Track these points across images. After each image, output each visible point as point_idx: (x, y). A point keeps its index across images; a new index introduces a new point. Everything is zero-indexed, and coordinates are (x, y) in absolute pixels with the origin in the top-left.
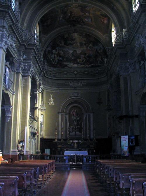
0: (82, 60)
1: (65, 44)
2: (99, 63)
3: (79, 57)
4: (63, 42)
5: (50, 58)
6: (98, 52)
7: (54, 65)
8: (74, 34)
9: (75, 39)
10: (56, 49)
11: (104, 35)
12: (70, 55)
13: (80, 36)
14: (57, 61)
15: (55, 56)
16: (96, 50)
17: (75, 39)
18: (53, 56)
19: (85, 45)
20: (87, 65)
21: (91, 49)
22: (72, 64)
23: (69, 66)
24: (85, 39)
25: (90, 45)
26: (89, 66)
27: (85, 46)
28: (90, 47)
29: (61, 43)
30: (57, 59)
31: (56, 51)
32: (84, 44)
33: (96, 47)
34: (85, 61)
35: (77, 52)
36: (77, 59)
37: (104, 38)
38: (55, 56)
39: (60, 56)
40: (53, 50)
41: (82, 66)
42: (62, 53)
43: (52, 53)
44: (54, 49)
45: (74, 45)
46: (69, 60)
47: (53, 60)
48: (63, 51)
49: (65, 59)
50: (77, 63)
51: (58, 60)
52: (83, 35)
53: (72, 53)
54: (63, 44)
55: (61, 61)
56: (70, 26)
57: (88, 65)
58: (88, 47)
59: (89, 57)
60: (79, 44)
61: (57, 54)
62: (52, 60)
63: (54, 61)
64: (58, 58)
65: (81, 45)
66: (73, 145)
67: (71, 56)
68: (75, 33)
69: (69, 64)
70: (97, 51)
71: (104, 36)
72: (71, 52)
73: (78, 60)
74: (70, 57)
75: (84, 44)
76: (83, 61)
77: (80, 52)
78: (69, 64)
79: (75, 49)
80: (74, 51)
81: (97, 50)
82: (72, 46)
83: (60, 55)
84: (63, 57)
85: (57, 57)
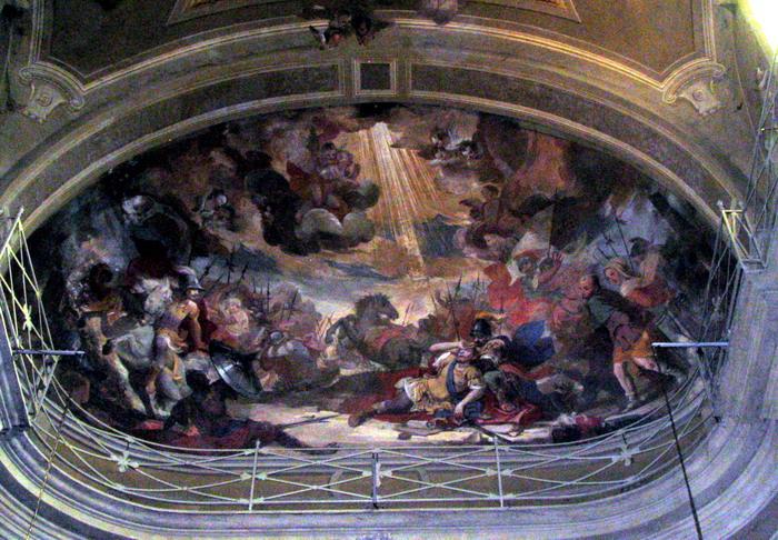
0: (450, 384)
1: (271, 235)
2: (629, 394)
3: (413, 360)
4: (257, 220)
5: (107, 349)
6: (613, 299)
7: (141, 417)
8: (362, 133)
9: (373, 194)
10: (183, 279)
11: (661, 80)
12: (329, 341)
13: (427, 153)
14: (177, 389)
15: (167, 339)
16: (585, 281)
17: (373, 194)
18: (142, 335)
19: (476, 240)
20: (507, 428)
21: (535, 283)
22: (340, 422)
23: (307, 436)
24: (475, 187)
25: (528, 241)
26: (531, 433)
27: (472, 254)
28: (532, 256)
29: (233, 228)
30: (181, 377)
31: (181, 293)
32: (460, 238)
33: (586, 254)
34: (476, 388)
35: (395, 315)
36: (395, 375)
37: (672, 98)
38: (167, 339)
39: (218, 350)
40: (150, 283)
41: (445, 436)
42: (234, 322)
43: (135, 308)
44: (158, 276)
45: (369, 247)
46: (308, 386)
47: (140, 376)
48: (250, 301)
49: (268, 380)
50: (399, 413)
51: (194, 378)
52: (453, 144)
53: (341, 323)
54: (252, 238)
55: (224, 390)
56: (321, 24)
57: (520, 432)
58: (504, 258)
59: (522, 353)
60: (410, 241)
61: (186, 325)
62: (124, 373)
63: (151, 386)
64: (196, 362)
65: (438, 239)
66: (194, 437)
67: (330, 349)
68: (380, 128)
69: (311, 420)
70: (600, 291)
71: (663, 87)
72: (335, 310)
73: (410, 388)
74: (320, 363)
75: (460, 238)
76: (457, 394)
77: (429, 308)
78: (311, 420)
79: (379, 288)
80: (362, 305)
81: (596, 281)
82: (339, 260)
83: (218, 337)
84: (245, 362)
85: (183, 356)
